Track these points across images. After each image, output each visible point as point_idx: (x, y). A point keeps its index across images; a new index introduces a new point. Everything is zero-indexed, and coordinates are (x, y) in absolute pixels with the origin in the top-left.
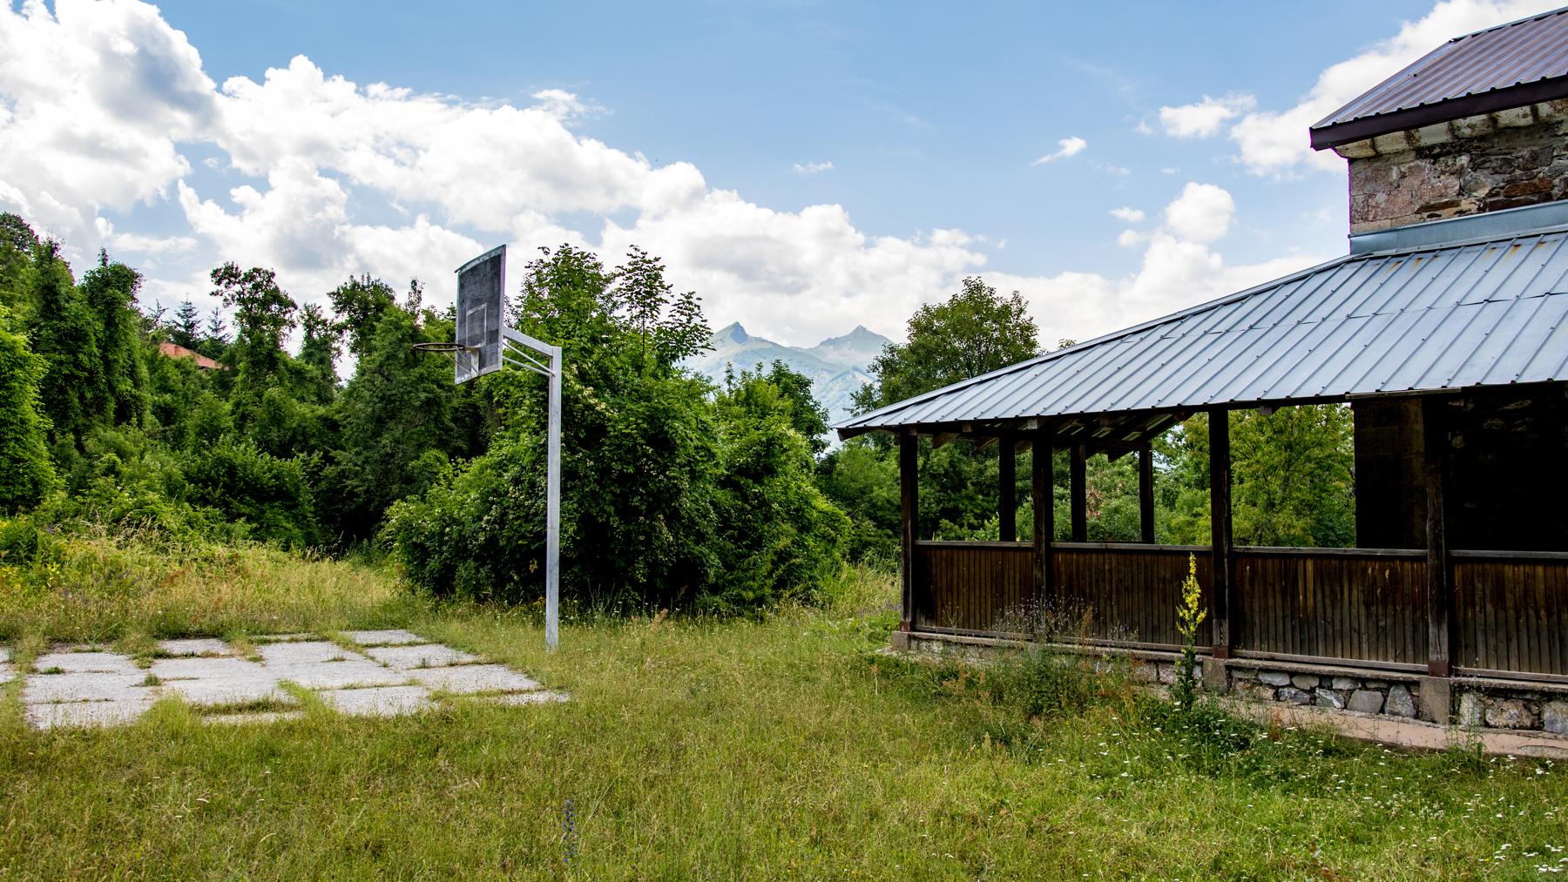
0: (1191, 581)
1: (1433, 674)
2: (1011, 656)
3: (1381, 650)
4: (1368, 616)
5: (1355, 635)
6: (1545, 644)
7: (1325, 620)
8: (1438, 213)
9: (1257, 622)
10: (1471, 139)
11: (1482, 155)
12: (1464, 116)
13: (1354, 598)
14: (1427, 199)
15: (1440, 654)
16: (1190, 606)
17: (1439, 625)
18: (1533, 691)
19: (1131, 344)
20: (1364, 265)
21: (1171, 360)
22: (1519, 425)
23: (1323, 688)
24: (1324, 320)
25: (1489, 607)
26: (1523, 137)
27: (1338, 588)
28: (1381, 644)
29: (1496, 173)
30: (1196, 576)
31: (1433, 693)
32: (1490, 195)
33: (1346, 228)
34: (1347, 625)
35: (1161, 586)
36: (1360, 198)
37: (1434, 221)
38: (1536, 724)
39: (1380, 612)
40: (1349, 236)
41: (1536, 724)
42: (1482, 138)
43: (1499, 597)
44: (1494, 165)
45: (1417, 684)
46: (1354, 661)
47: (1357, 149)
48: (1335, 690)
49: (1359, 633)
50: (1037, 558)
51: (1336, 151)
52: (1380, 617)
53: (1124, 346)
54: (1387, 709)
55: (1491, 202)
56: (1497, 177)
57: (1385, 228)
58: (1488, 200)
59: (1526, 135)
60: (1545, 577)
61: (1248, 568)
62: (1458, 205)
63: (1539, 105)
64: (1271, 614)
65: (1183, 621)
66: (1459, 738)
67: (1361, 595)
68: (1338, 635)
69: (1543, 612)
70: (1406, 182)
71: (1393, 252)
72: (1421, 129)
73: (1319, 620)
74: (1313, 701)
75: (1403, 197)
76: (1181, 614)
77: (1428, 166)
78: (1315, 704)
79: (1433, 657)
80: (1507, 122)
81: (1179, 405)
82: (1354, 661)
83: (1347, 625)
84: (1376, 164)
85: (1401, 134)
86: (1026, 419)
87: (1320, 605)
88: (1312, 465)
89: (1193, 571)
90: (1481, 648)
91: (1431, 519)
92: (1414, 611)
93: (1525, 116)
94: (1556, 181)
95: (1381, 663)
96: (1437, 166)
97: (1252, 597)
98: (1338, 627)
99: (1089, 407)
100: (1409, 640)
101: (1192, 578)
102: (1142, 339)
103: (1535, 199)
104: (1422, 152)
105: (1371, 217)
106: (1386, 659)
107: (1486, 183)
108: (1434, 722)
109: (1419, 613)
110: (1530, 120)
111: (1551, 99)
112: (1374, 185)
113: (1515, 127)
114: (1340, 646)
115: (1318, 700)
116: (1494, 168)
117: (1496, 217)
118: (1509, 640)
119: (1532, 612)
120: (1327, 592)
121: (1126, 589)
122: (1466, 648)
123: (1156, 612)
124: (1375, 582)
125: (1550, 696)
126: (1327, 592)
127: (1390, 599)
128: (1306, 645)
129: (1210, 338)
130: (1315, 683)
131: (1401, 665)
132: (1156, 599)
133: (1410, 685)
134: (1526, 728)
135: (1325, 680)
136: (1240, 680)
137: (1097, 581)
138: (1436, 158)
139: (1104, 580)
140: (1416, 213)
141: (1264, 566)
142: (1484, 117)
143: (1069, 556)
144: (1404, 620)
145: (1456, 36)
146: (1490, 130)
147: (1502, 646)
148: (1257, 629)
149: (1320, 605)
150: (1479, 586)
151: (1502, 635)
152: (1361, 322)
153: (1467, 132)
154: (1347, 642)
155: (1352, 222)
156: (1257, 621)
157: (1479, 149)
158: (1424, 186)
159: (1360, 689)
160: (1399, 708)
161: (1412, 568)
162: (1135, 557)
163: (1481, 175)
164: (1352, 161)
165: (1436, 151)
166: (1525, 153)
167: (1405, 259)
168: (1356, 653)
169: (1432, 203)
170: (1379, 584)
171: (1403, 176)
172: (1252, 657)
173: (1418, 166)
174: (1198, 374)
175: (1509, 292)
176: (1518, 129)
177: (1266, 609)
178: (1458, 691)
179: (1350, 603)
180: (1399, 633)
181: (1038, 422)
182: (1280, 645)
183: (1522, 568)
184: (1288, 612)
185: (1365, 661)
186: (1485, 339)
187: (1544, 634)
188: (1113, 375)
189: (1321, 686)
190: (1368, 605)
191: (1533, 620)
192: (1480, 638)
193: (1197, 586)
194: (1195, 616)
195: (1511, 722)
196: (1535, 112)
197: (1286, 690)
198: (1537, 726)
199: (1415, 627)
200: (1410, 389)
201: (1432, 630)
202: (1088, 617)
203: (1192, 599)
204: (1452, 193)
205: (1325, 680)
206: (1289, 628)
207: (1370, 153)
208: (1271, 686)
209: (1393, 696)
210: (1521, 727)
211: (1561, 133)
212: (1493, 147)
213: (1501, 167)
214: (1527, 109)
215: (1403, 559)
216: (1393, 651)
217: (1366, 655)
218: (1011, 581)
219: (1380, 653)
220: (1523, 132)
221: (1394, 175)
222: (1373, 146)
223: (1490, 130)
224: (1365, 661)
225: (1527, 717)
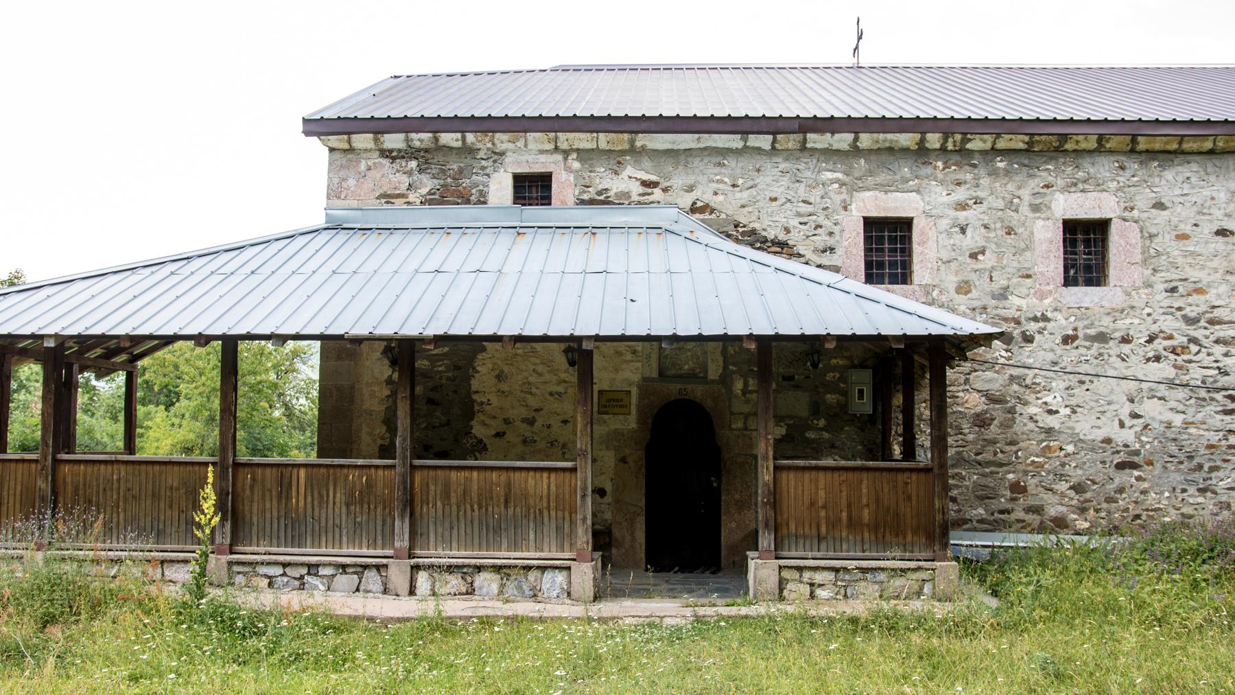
0: (209, 490)
1: (397, 558)
2: (16, 565)
3: (357, 541)
4: (348, 513)
5: (337, 530)
6: (476, 530)
7: (313, 518)
8: (392, 201)
9: (256, 523)
10: (419, 150)
11: (426, 163)
12: (417, 132)
13: (338, 500)
14: (385, 190)
15: (402, 542)
16: (206, 511)
17: (402, 517)
18: (469, 566)
19: (143, 276)
20: (337, 233)
21: (184, 294)
22: (440, 366)
23: (311, 575)
24: (314, 272)
25: (439, 504)
26: (454, 155)
27: (325, 492)
28: (357, 537)
29: (435, 178)
30: (213, 484)
31: (398, 573)
32: (430, 193)
33: (323, 201)
34: (331, 522)
35: (168, 494)
36: (336, 181)
37: (389, 206)
38: (470, 591)
39: (358, 510)
40: (325, 209)
41: (470, 591)
42: (426, 151)
43: (446, 496)
44: (434, 172)
45: (386, 566)
46: (336, 551)
47: (337, 141)
48: (320, 576)
49: (340, 528)
50: (42, 470)
51: (320, 139)
52: (357, 515)
53: (135, 278)
54: (362, 588)
55: (430, 199)
56: (435, 180)
57: (353, 207)
58: (428, 197)
59: (457, 154)
60: (478, 480)
61: (249, 476)
62: (407, 198)
63: (467, 134)
64: (268, 515)
65: (199, 526)
66: (429, 608)
67: (343, 498)
68: (323, 530)
69: (476, 506)
70: (370, 174)
71: (359, 226)
72: (385, 135)
73: (308, 519)
74: (302, 587)
75: (368, 185)
76: (197, 519)
77: (388, 164)
78: (303, 589)
79: (397, 544)
80: (445, 142)
81: (200, 333)
82: (336, 551)
83: (331, 522)
84: (350, 156)
85: (371, 136)
86: (42, 337)
87: (309, 506)
88: (247, 389)
89: (210, 480)
90: (432, 535)
91: (400, 436)
92: (384, 508)
93: (457, 140)
94: (474, 191)
95: (357, 551)
96: (394, 165)
97: (252, 502)
98: (323, 524)
99: (110, 330)
100: (379, 532)
101: (210, 486)
102: (152, 273)
103: (460, 201)
104: (386, 154)
105: (343, 197)
106: (361, 548)
107: (427, 184)
108: (398, 595)
109: (387, 510)
110: (459, 144)
111: (476, 132)
112: (347, 171)
113: (448, 147)
114: (324, 539)
115: (306, 585)
116: (433, 174)
117: (432, 210)
118: (452, 528)
119: (468, 507)
120: (316, 495)
121: (134, 497)
122: (421, 535)
123: (162, 518)
124: (354, 486)
125: (479, 569)
126: (316, 495)
127: (366, 499)
128: (297, 540)
129: (216, 279)
130: (304, 571)
131: (372, 552)
132: (162, 505)
133: (378, 567)
134: (463, 594)
135: (312, 568)
136: (239, 573)
137: (105, 490)
138: (394, 159)
139: (112, 489)
140: (377, 198)
141: (263, 474)
142: (430, 135)
143: (76, 467)
144: (376, 516)
145: (397, 75)
146: (433, 146)
147: (447, 533)
148: (255, 529)
149: (309, 506)
150: (432, 487)
151: (447, 525)
152: (301, 278)
153: (417, 144)
154: (330, 535)
155: (328, 198)
156: (255, 519)
157: (424, 157)
158: (383, 179)
159: (341, 574)
160: (371, 587)
161: (384, 475)
162: (143, 467)
163: (424, 178)
164: (332, 150)
165: (394, 154)
166: (455, 167)
167: (369, 232)
168: (337, 545)
169: (389, 192)
170: (358, 488)
171: (369, 169)
172: (253, 551)
173: (381, 163)
174: (211, 308)
175: (451, 266)
176: (451, 148)
177: (264, 511)
178: (416, 568)
179: (334, 503)
180: (371, 525)
181: (56, 341)
182: (275, 541)
183: (463, 474)
184: (283, 513)
185: (323, 550)
186: (262, 301)
187: (476, 523)
188: (129, 302)
189: (309, 574)
190: (348, 505)
191: (469, 512)
192: (432, 528)
193: (213, 494)
194: (210, 520)
195: (453, 591)
196: (464, 139)
197: (279, 578)
198: (471, 592)
199: (384, 521)
200: (396, 333)
201: (397, 523)
202: (98, 526)
203: (208, 505)
204: (403, 188)
205: (312, 568)
206: (283, 526)
207: (346, 146)
208: (266, 576)
209: (367, 578)
210: (460, 594)
211: (479, 157)
212: (433, 158)
213: (438, 174)
214: (459, 135)
215: (377, 467)
216: (366, 541)
217: (345, 545)
218: (11, 492)
219: (357, 544)
220: (454, 151)
221: (363, 166)
222: (349, 142)
223: (433, 146)
224: (345, 551)
225: (464, 585)
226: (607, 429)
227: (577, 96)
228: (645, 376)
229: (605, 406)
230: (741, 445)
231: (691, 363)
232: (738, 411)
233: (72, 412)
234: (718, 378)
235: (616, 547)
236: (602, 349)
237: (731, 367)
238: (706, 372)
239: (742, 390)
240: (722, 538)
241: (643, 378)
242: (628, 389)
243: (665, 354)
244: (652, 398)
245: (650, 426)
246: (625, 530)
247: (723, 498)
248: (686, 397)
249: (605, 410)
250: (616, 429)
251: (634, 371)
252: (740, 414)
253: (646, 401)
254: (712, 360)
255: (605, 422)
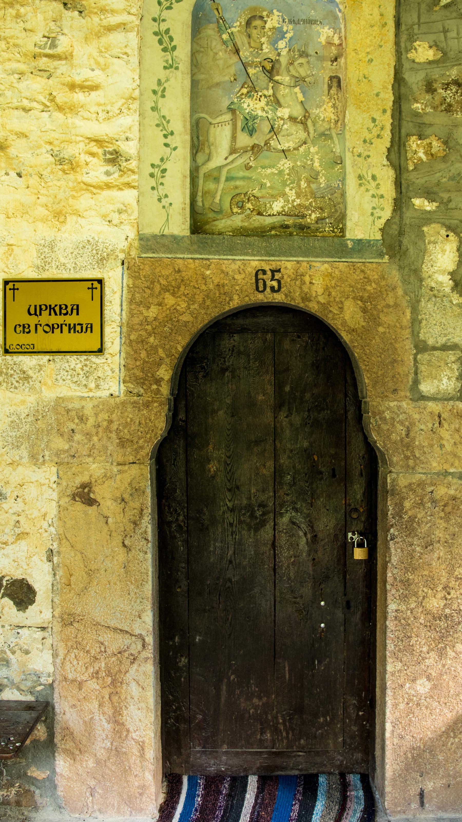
226: (32, 399)
227: (223, 189)
228: (147, 231)
229: (25, 329)
230: (448, 447)
231: (292, 195)
232: (442, 341)
233: (290, 307)
234: (378, 236)
235: (69, 753)
236: (12, 151)
237: (417, 202)
238: (342, 218)
239: (453, 274)
240: (388, 726)
241: (141, 238)
242: (96, 274)
243: (212, 164)
244: (170, 300)
245: (165, 390)
246: (96, 704)
247: (392, 607)
248: (279, 298)
249: (24, 339)
250: (59, 400)
251: (115, 218)
252: (445, 348)
253: (153, 312)
254: (360, 177)
255: (27, 378)
